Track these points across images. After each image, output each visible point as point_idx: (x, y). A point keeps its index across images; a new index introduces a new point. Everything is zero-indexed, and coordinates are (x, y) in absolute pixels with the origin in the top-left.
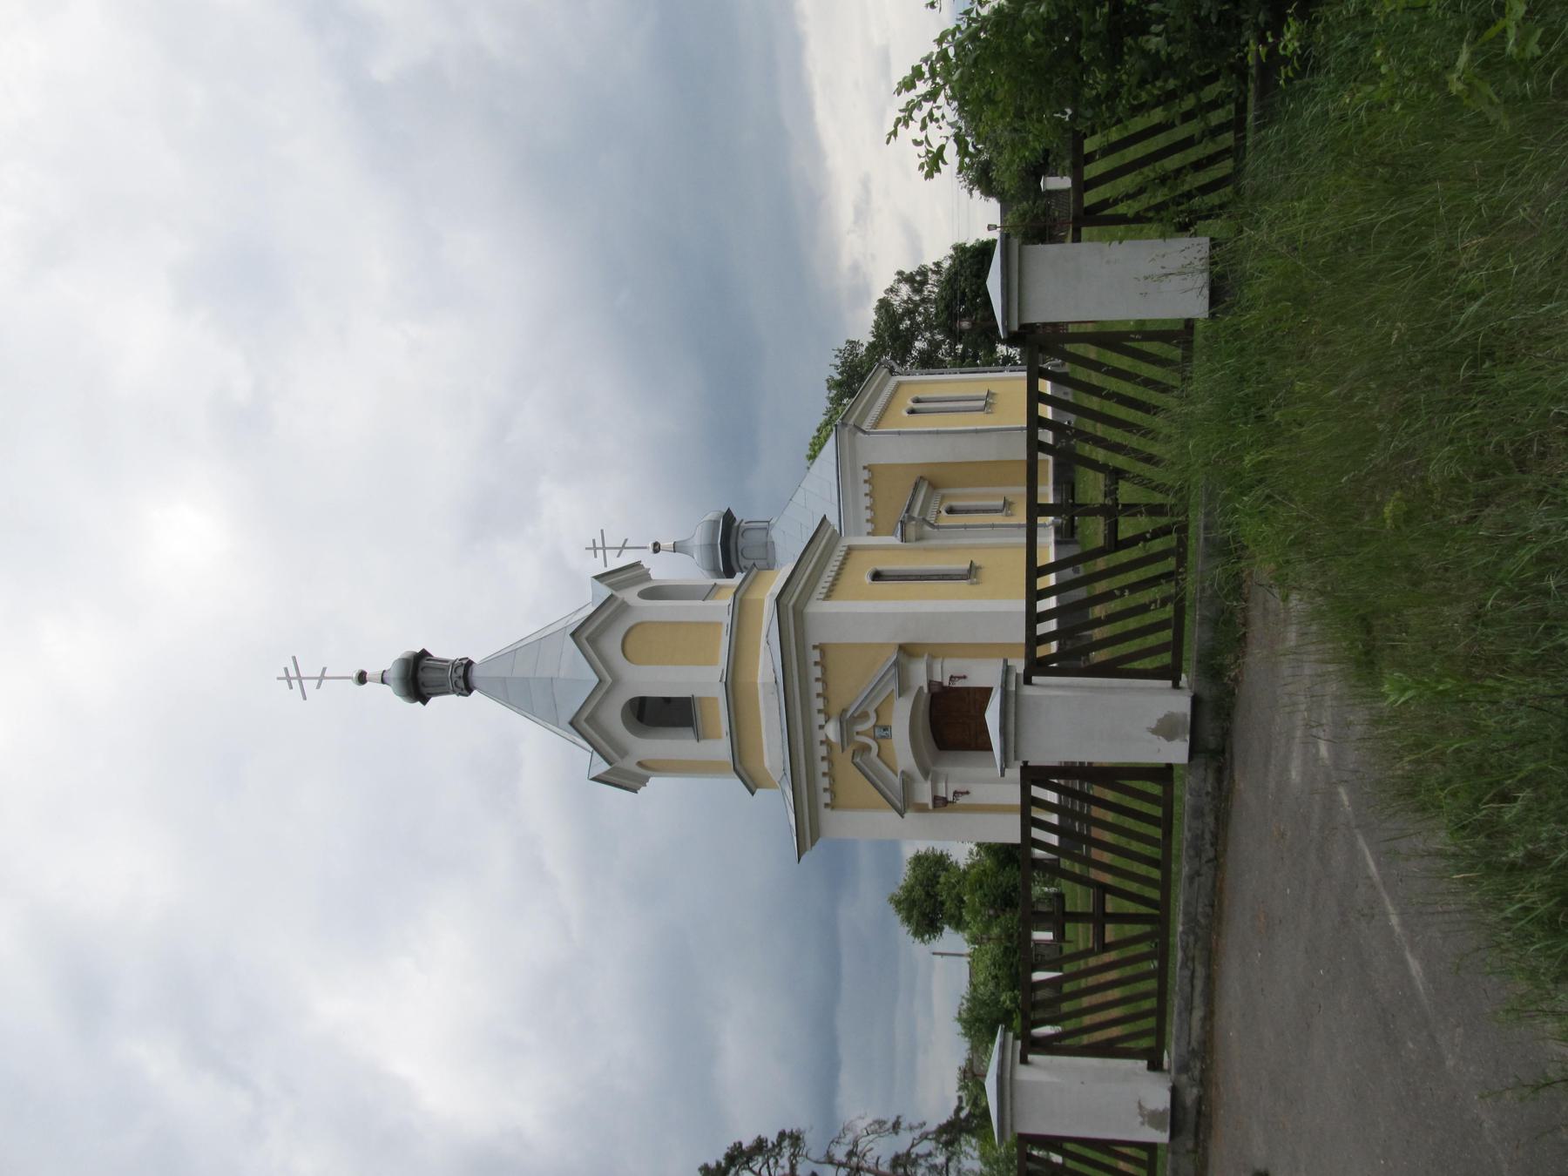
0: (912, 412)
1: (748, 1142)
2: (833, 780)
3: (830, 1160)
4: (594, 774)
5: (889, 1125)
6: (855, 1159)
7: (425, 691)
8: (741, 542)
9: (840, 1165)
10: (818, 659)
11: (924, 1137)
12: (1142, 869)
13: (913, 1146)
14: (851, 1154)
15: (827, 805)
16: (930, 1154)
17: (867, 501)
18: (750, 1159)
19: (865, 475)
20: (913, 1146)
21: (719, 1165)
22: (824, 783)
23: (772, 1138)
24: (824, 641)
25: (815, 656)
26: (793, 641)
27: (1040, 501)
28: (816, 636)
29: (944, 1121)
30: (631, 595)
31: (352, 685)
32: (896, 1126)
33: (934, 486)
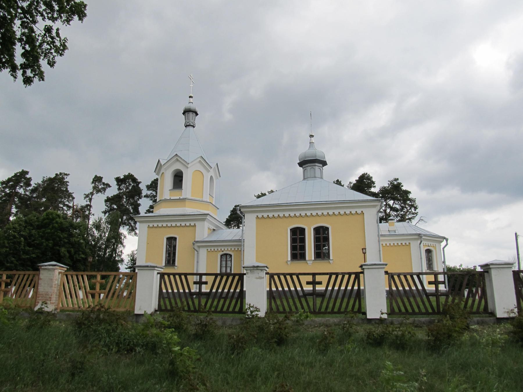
2: (156, 227)
4: (160, 160)
7: (186, 114)
10: (163, 226)
12: (331, 305)
15: (149, 226)
25: (192, 224)
26: (192, 218)
27: (316, 285)
30: (212, 173)
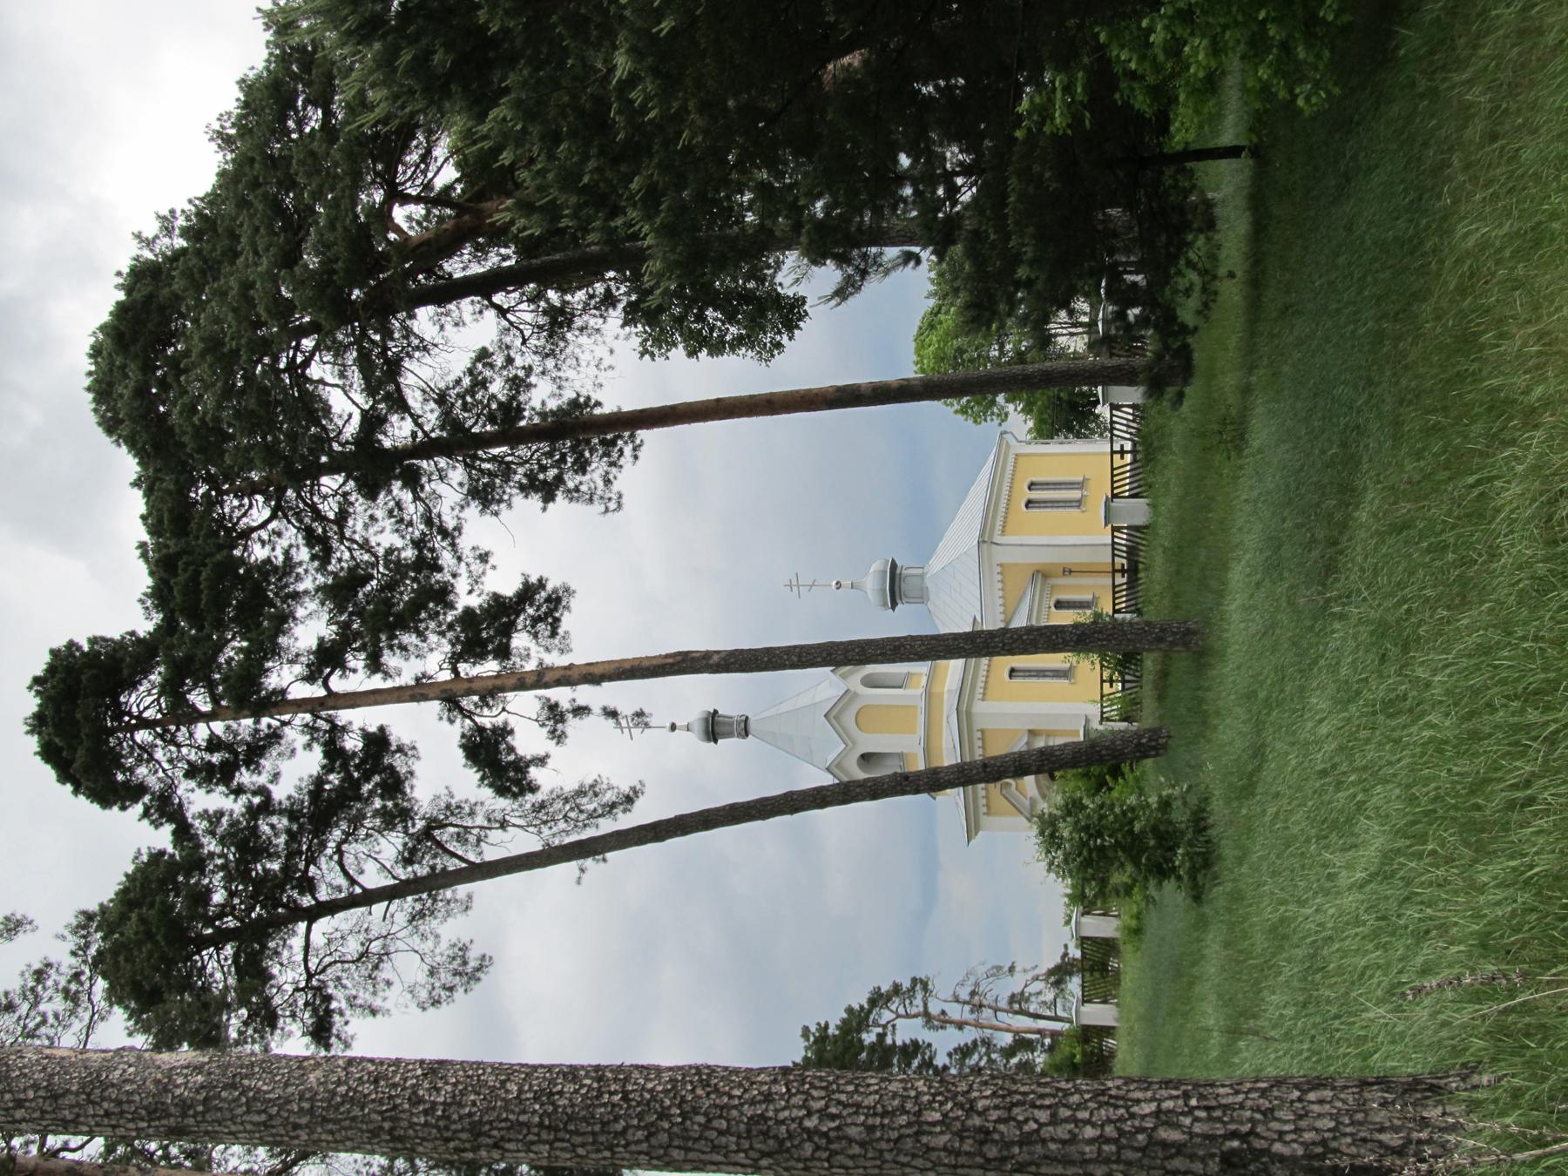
0: (1029, 503)
1: (886, 987)
3: (957, 1000)
5: (1006, 969)
6: (977, 998)
8: (903, 585)
9: (965, 1003)
11: (1036, 978)
13: (1026, 986)
14: (973, 993)
16: (1039, 993)
17: (1000, 585)
18: (889, 1000)
19: (999, 569)
20: (1026, 986)
21: (862, 1007)
22: (984, 801)
23: (906, 984)
24: (984, 727)
25: (979, 735)
28: (979, 724)
29: (1051, 966)
31: (666, 732)
32: (1012, 969)
33: (1046, 576)
